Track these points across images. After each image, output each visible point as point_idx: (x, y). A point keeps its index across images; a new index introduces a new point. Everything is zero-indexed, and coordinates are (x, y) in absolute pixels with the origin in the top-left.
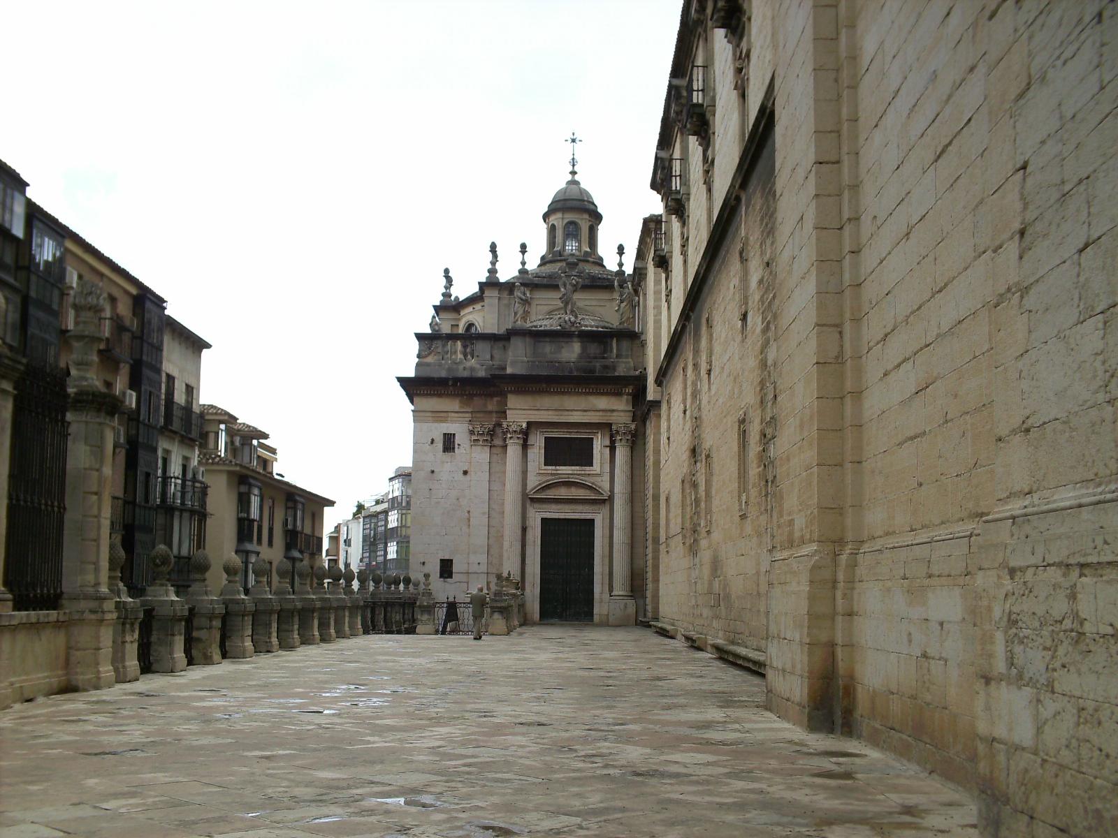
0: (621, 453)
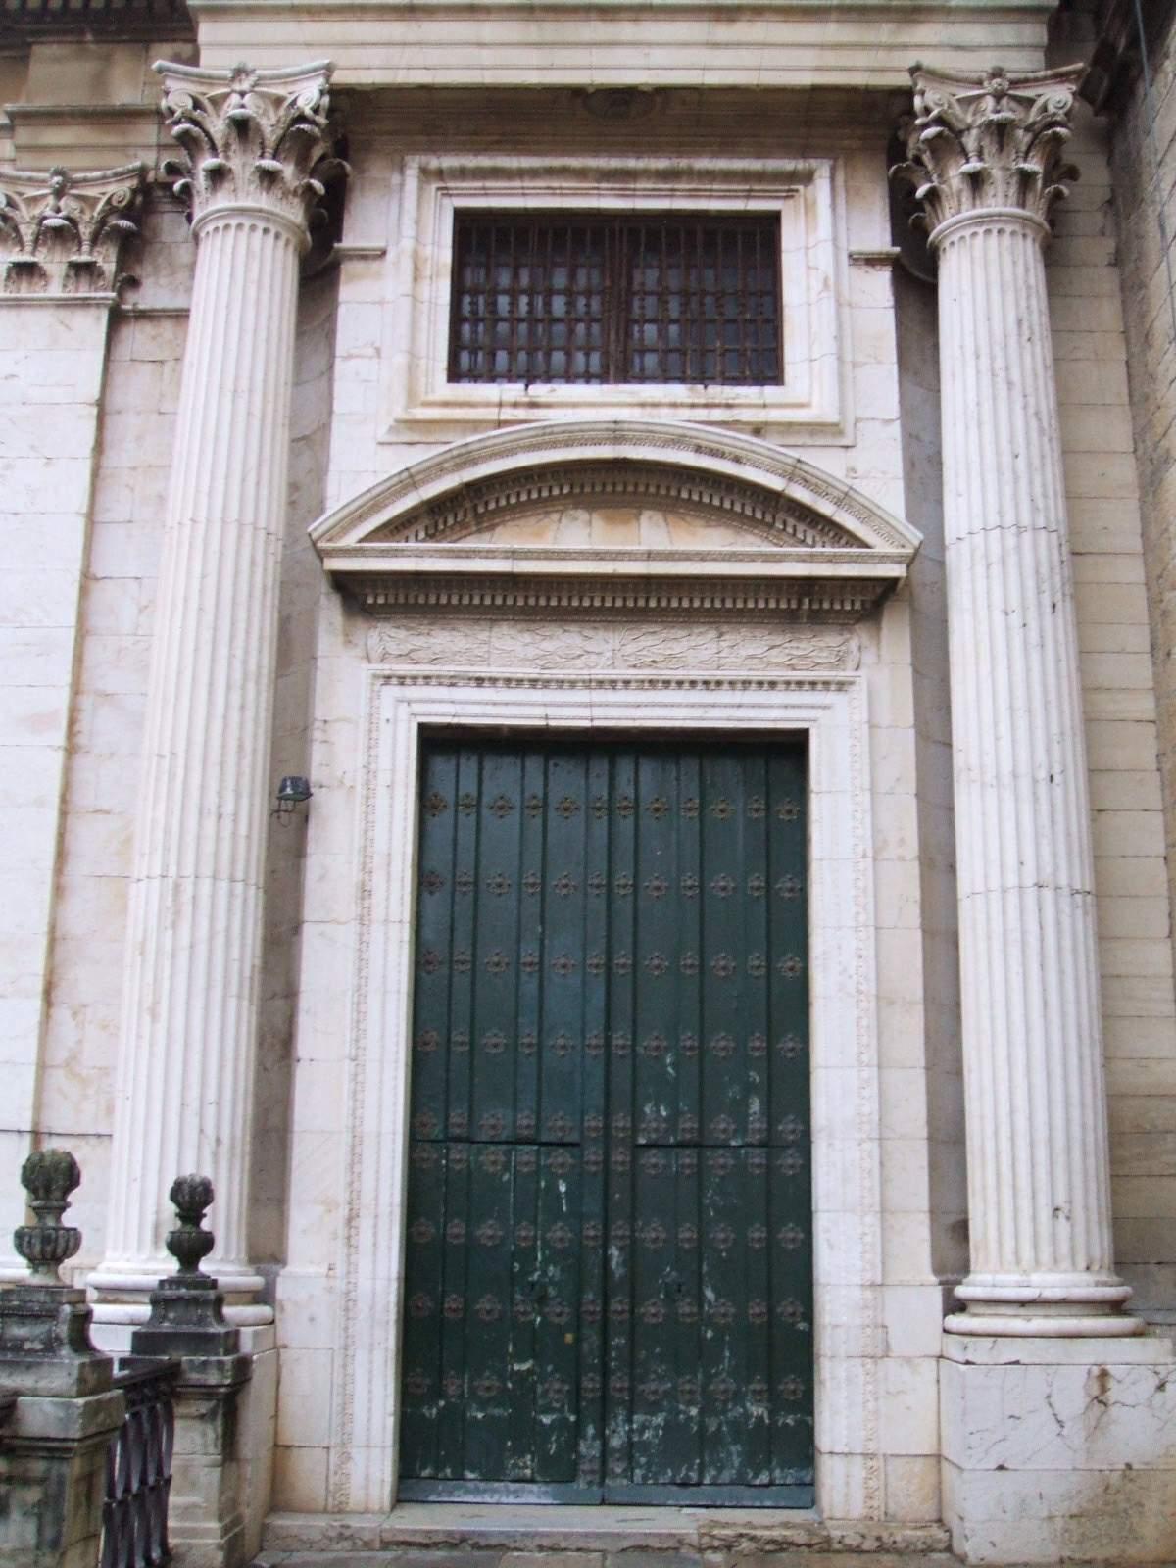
0: (987, 273)
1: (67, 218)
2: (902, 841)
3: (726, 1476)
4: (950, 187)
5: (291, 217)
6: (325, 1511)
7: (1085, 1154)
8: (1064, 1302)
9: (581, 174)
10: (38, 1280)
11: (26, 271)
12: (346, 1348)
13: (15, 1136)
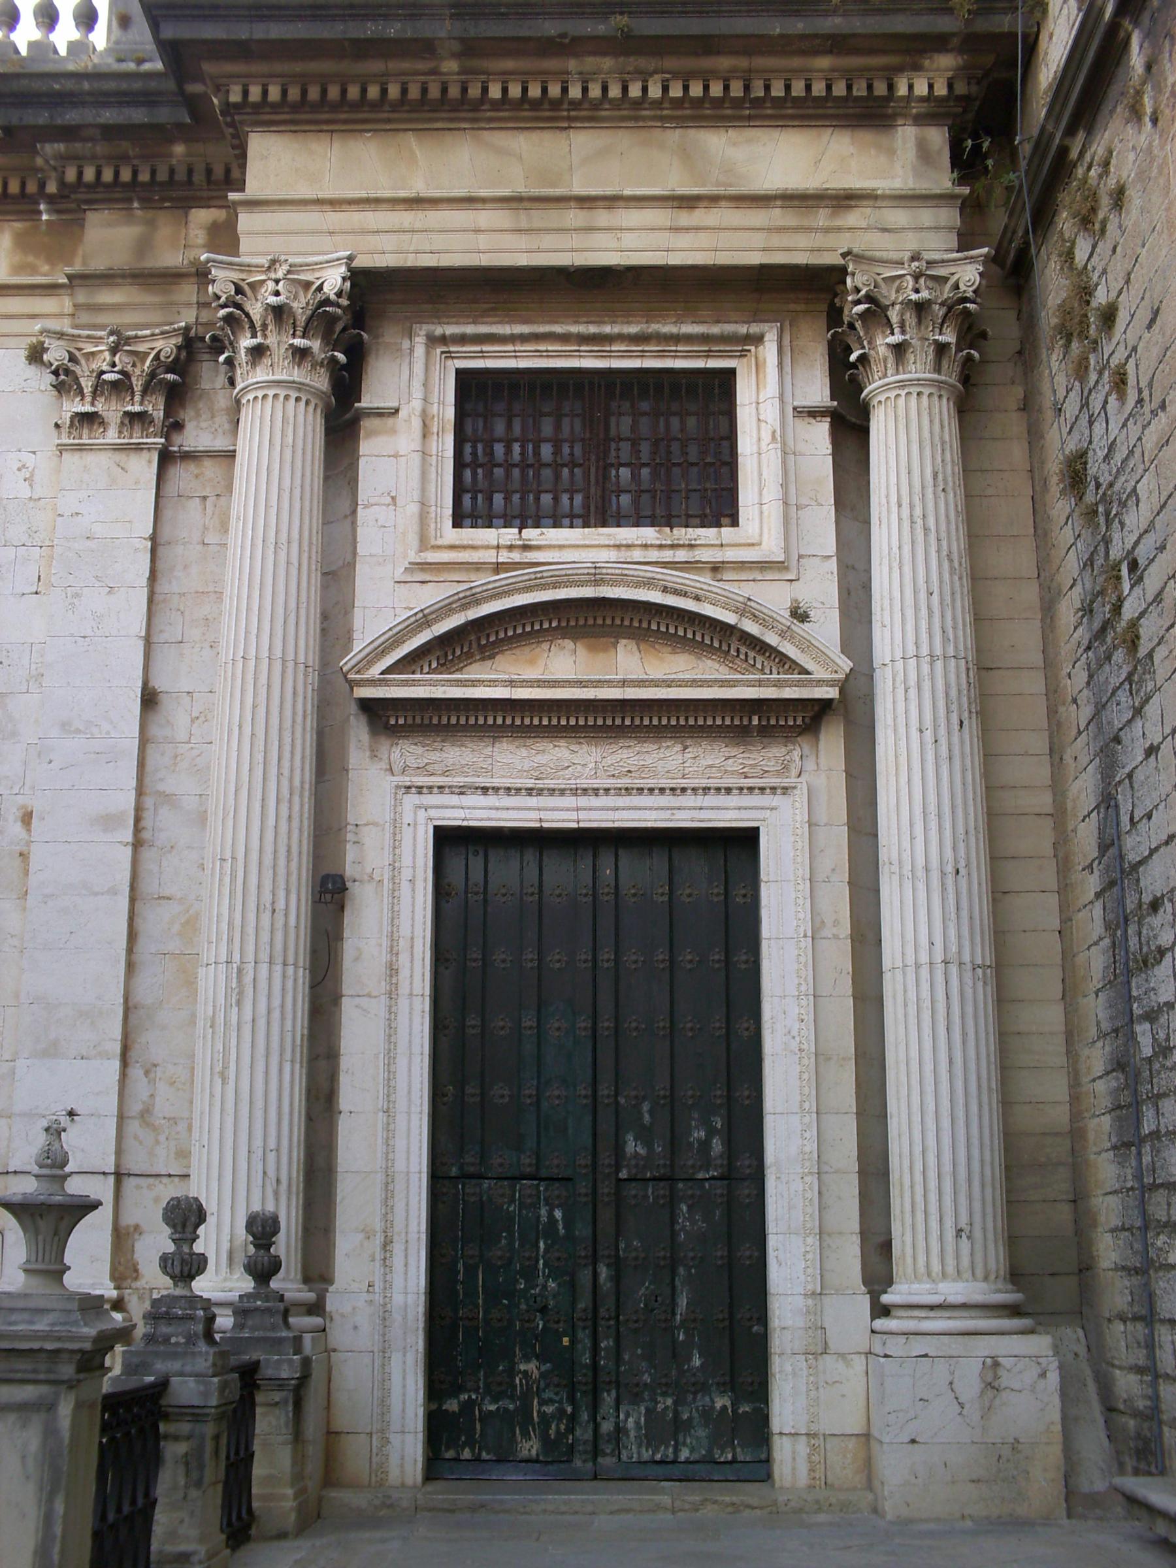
0: (907, 428)
1: (121, 372)
2: (836, 923)
4: (877, 353)
5: (318, 385)
7: (983, 1186)
8: (964, 1306)
9: (565, 338)
10: (178, 1292)
11: (88, 419)
13: (101, 1177)
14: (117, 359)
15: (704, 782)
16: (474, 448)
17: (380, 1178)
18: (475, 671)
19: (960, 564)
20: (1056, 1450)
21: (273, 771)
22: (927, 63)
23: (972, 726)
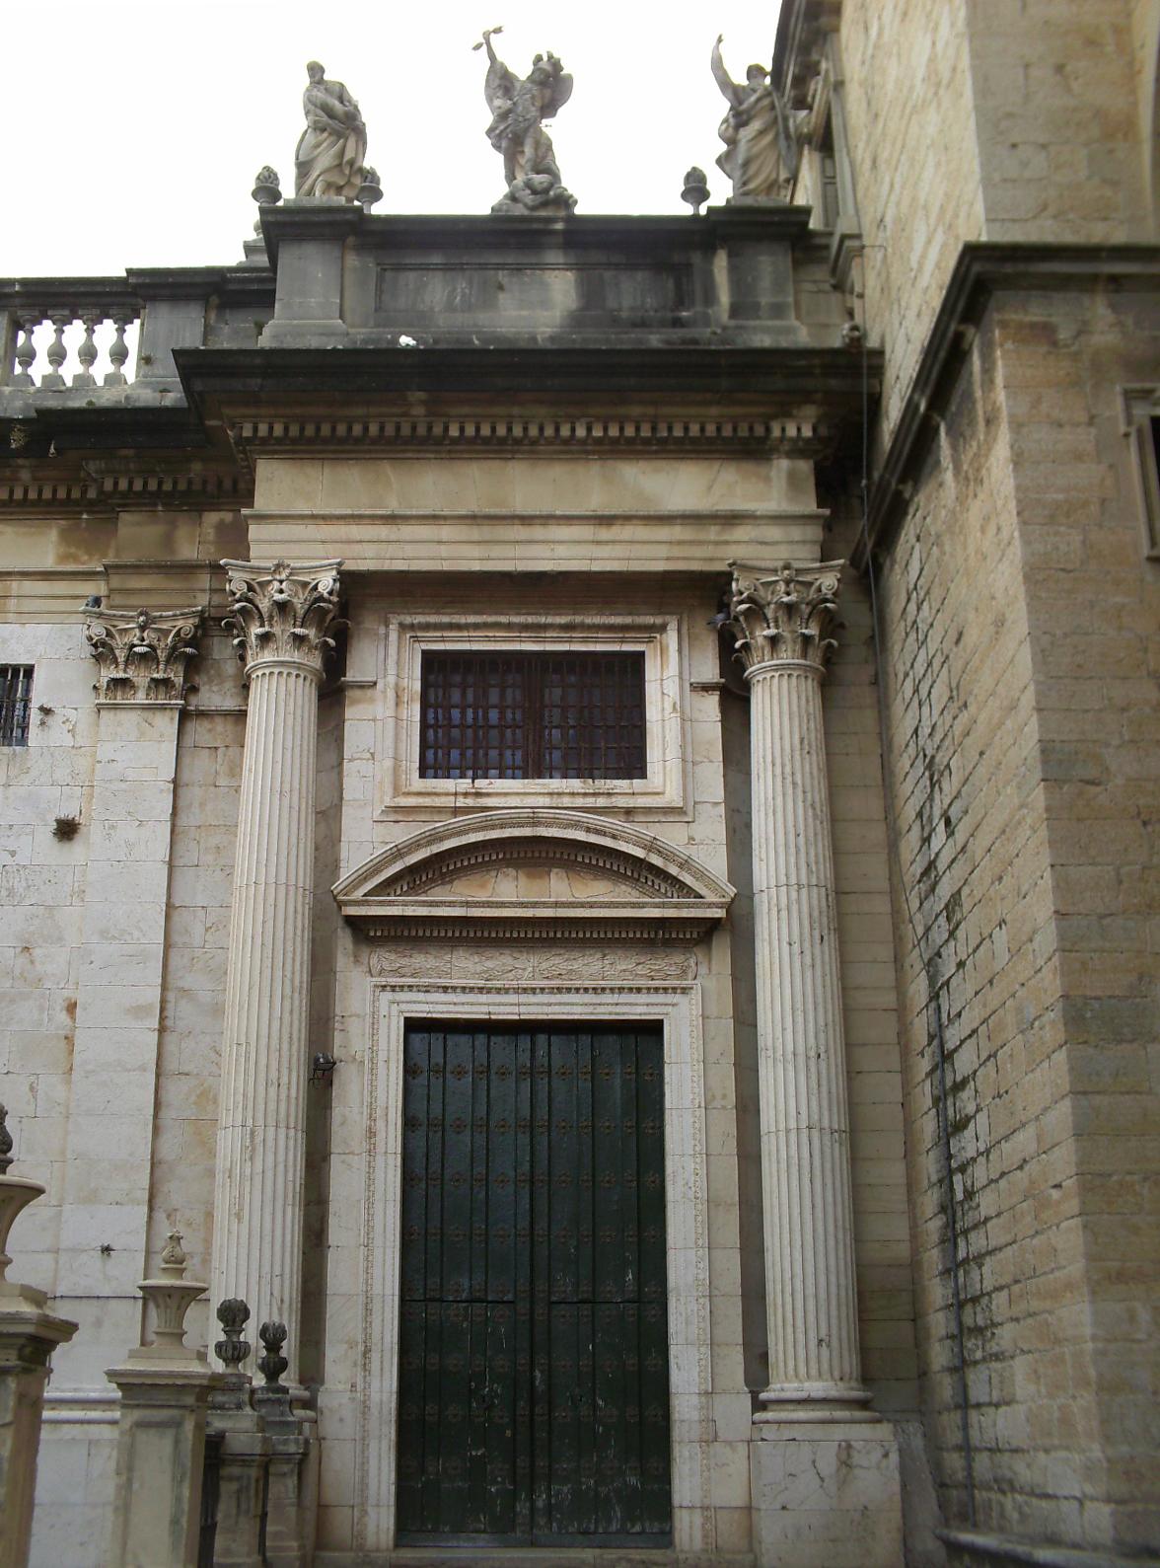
0: (779, 705)
2: (724, 1096)
3: (614, 1527)
6: (351, 1549)
9: (509, 627)
10: (230, 1371)
12: (363, 1439)
14: (145, 635)
15: (618, 983)
16: (436, 713)
17: (361, 1299)
18: (438, 894)
19: (822, 811)
20: (896, 1516)
21: (279, 974)
22: (795, 412)
23: (831, 940)
